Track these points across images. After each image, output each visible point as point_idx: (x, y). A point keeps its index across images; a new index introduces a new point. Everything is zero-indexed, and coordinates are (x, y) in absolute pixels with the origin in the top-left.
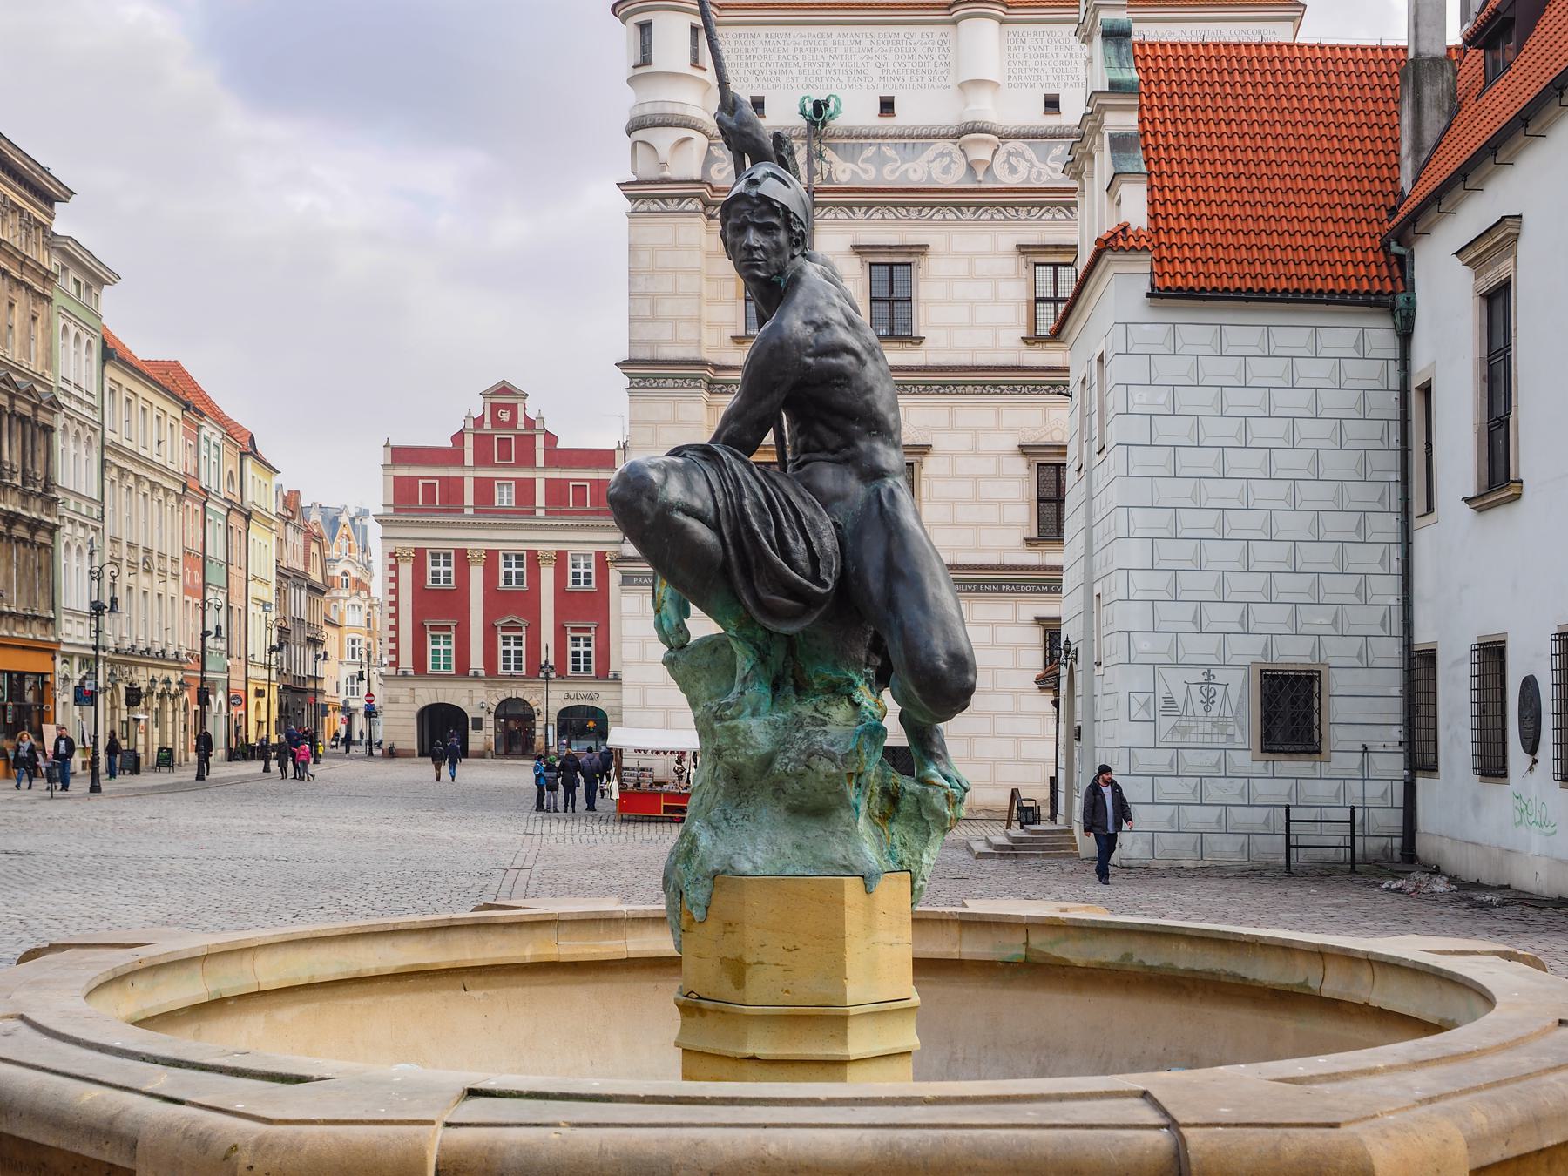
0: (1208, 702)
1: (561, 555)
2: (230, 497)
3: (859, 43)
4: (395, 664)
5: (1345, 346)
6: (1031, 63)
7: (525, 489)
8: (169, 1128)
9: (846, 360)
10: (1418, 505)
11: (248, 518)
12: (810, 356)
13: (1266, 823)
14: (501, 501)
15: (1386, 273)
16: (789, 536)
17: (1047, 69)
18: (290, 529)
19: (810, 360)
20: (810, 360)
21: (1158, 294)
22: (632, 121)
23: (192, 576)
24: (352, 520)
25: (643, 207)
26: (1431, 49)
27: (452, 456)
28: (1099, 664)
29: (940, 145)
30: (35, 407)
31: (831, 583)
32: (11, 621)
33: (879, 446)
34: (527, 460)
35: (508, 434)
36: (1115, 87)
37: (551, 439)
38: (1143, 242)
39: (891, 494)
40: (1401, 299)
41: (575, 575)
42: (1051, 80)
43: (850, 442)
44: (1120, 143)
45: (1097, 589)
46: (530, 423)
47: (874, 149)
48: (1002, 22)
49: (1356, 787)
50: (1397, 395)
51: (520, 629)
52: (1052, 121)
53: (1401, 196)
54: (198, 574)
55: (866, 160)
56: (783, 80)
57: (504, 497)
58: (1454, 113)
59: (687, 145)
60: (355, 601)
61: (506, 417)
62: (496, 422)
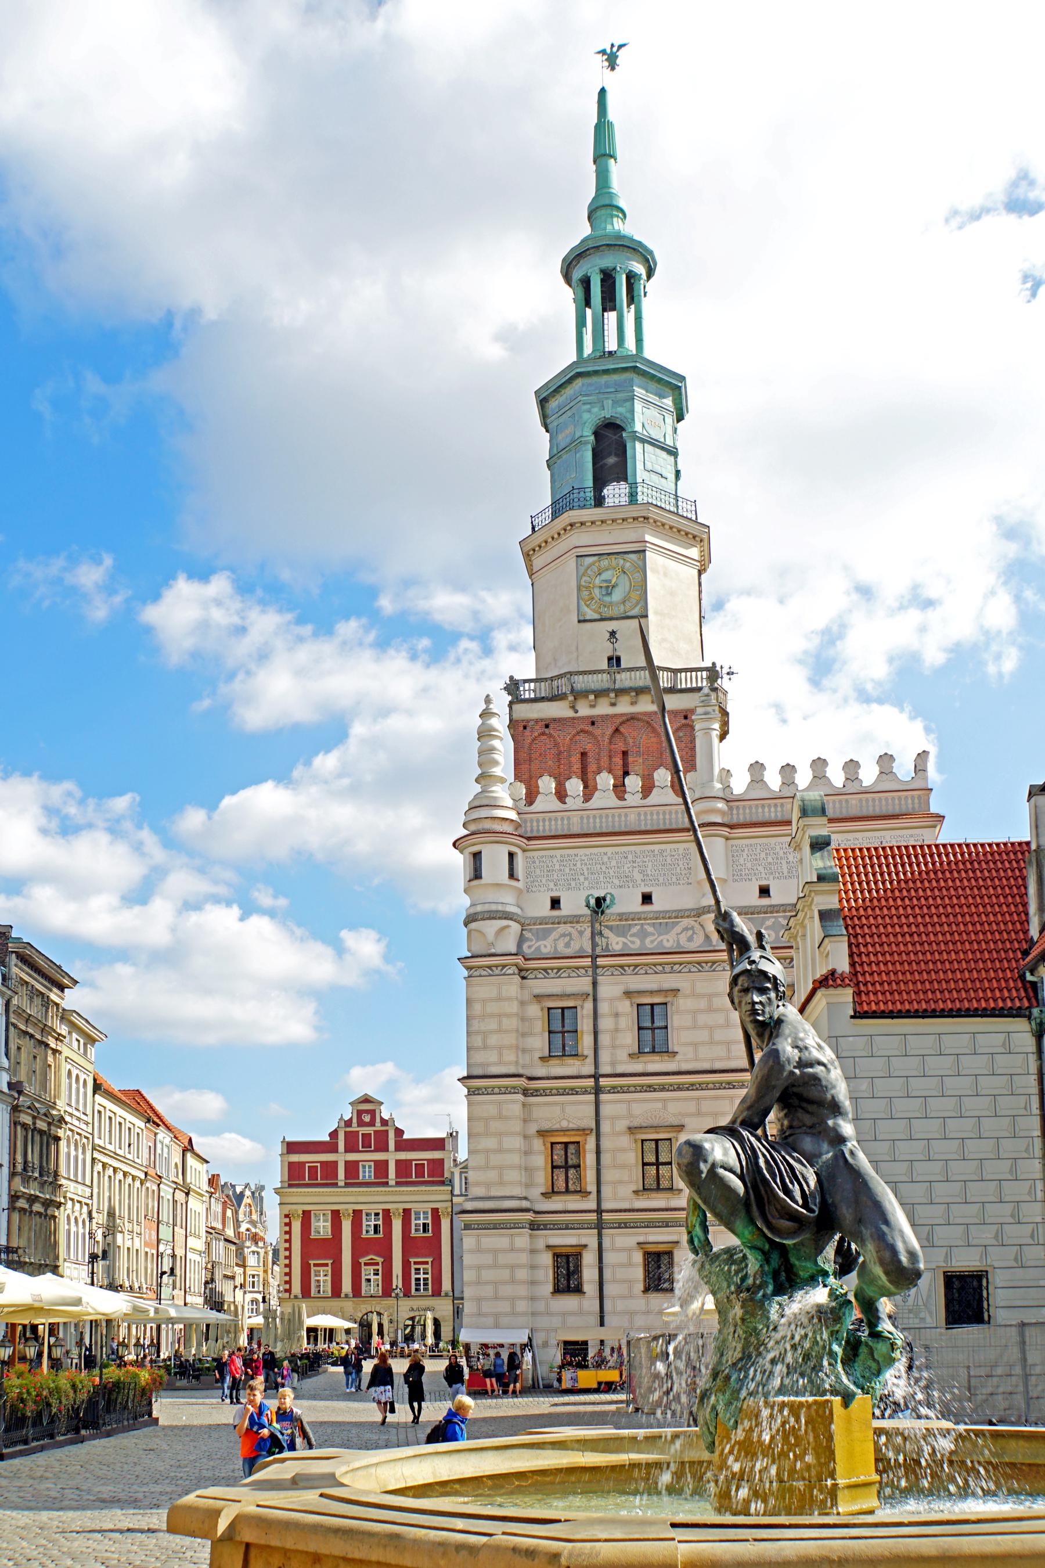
1: (407, 1212)
2: (176, 1180)
3: (626, 858)
4: (289, 1291)
6: (749, 865)
7: (381, 1167)
9: (819, 1069)
11: (187, 1194)
14: (364, 1176)
15: (1023, 994)
16: (787, 1181)
17: (760, 868)
21: (857, 1015)
22: (468, 917)
23: (150, 1234)
24: (253, 1193)
25: (477, 973)
27: (329, 1147)
29: (685, 922)
30: (49, 1124)
31: (817, 1209)
32: (31, 1268)
35: (364, 1130)
37: (399, 1132)
39: (852, 1153)
41: (416, 1225)
42: (763, 875)
44: (825, 916)
46: (384, 1122)
47: (638, 927)
48: (727, 839)
50: (1036, 1077)
51: (377, 1264)
52: (765, 901)
53: (1032, 943)
54: (154, 1233)
55: (632, 935)
56: (573, 884)
57: (367, 1173)
59: (507, 930)
60: (254, 1248)
61: (367, 1118)
62: (361, 1123)
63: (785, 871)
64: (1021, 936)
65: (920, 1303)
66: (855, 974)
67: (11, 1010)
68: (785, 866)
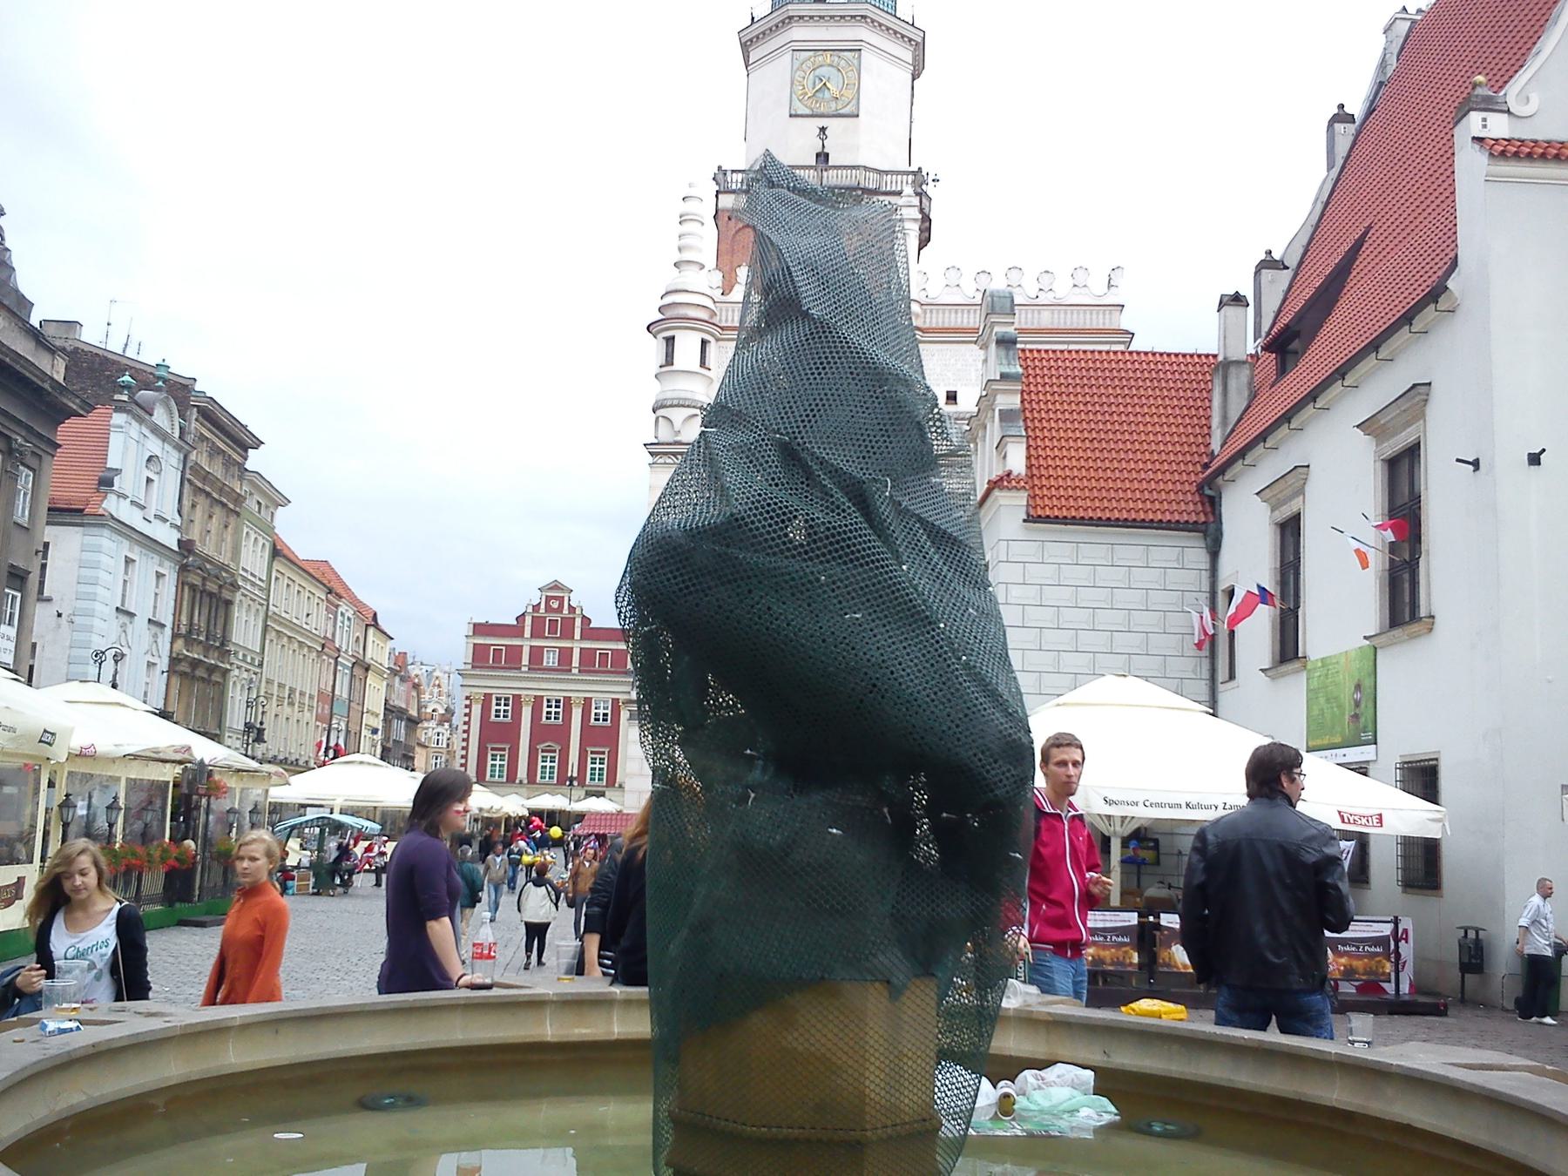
1: (588, 701)
5: (1174, 559)
7: (565, 655)
10: (1222, 673)
11: (367, 669)
18: (397, 679)
21: (1030, 519)
26: (1235, 355)
27: (515, 630)
34: (568, 634)
35: (554, 616)
36: (1004, 377)
37: (586, 620)
40: (1212, 527)
44: (1006, 416)
46: (572, 609)
53: (1212, 456)
54: (327, 707)
57: (550, 660)
58: (1253, 396)
61: (555, 605)
62: (548, 609)
67: (189, 465)
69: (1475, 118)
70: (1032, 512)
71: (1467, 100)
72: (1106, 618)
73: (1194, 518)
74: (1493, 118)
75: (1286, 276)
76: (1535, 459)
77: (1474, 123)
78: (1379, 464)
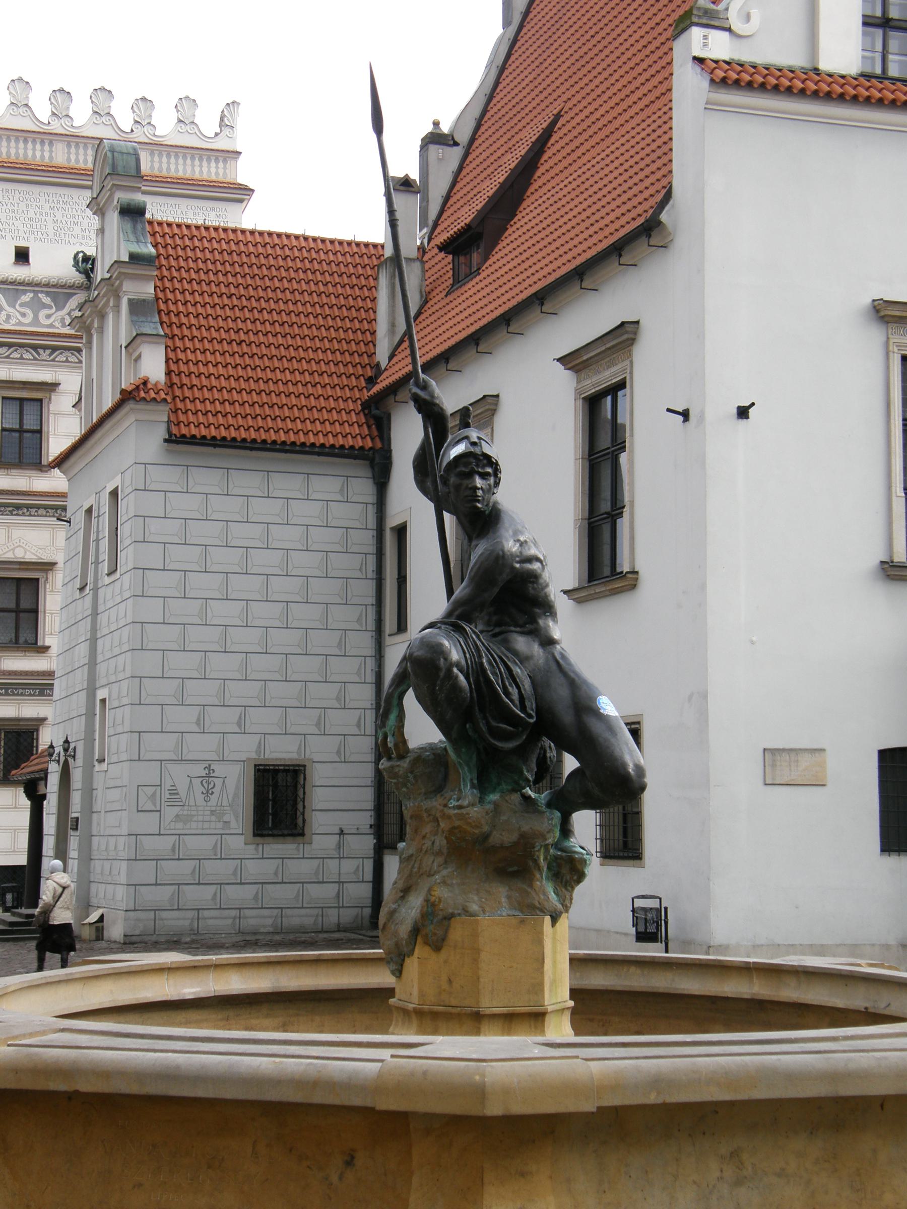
0: (208, 793)
8: (412, 1074)
9: (536, 566)
12: (518, 562)
13: (256, 898)
19: (518, 565)
20: (518, 565)
21: (172, 440)
28: (102, 761)
31: (534, 714)
33: (551, 624)
38: (163, 395)
42: (21, 234)
43: (533, 620)
44: (137, 307)
45: (101, 694)
49: (333, 864)
63: (51, 232)
64: (366, 360)
65: (225, 803)
66: (171, 385)
68: (50, 225)
69: (696, 33)
70: (175, 430)
71: (688, 14)
72: (263, 560)
73: (359, 443)
74: (714, 34)
75: (456, 154)
76: (743, 413)
77: (703, 42)
78: (580, 403)
